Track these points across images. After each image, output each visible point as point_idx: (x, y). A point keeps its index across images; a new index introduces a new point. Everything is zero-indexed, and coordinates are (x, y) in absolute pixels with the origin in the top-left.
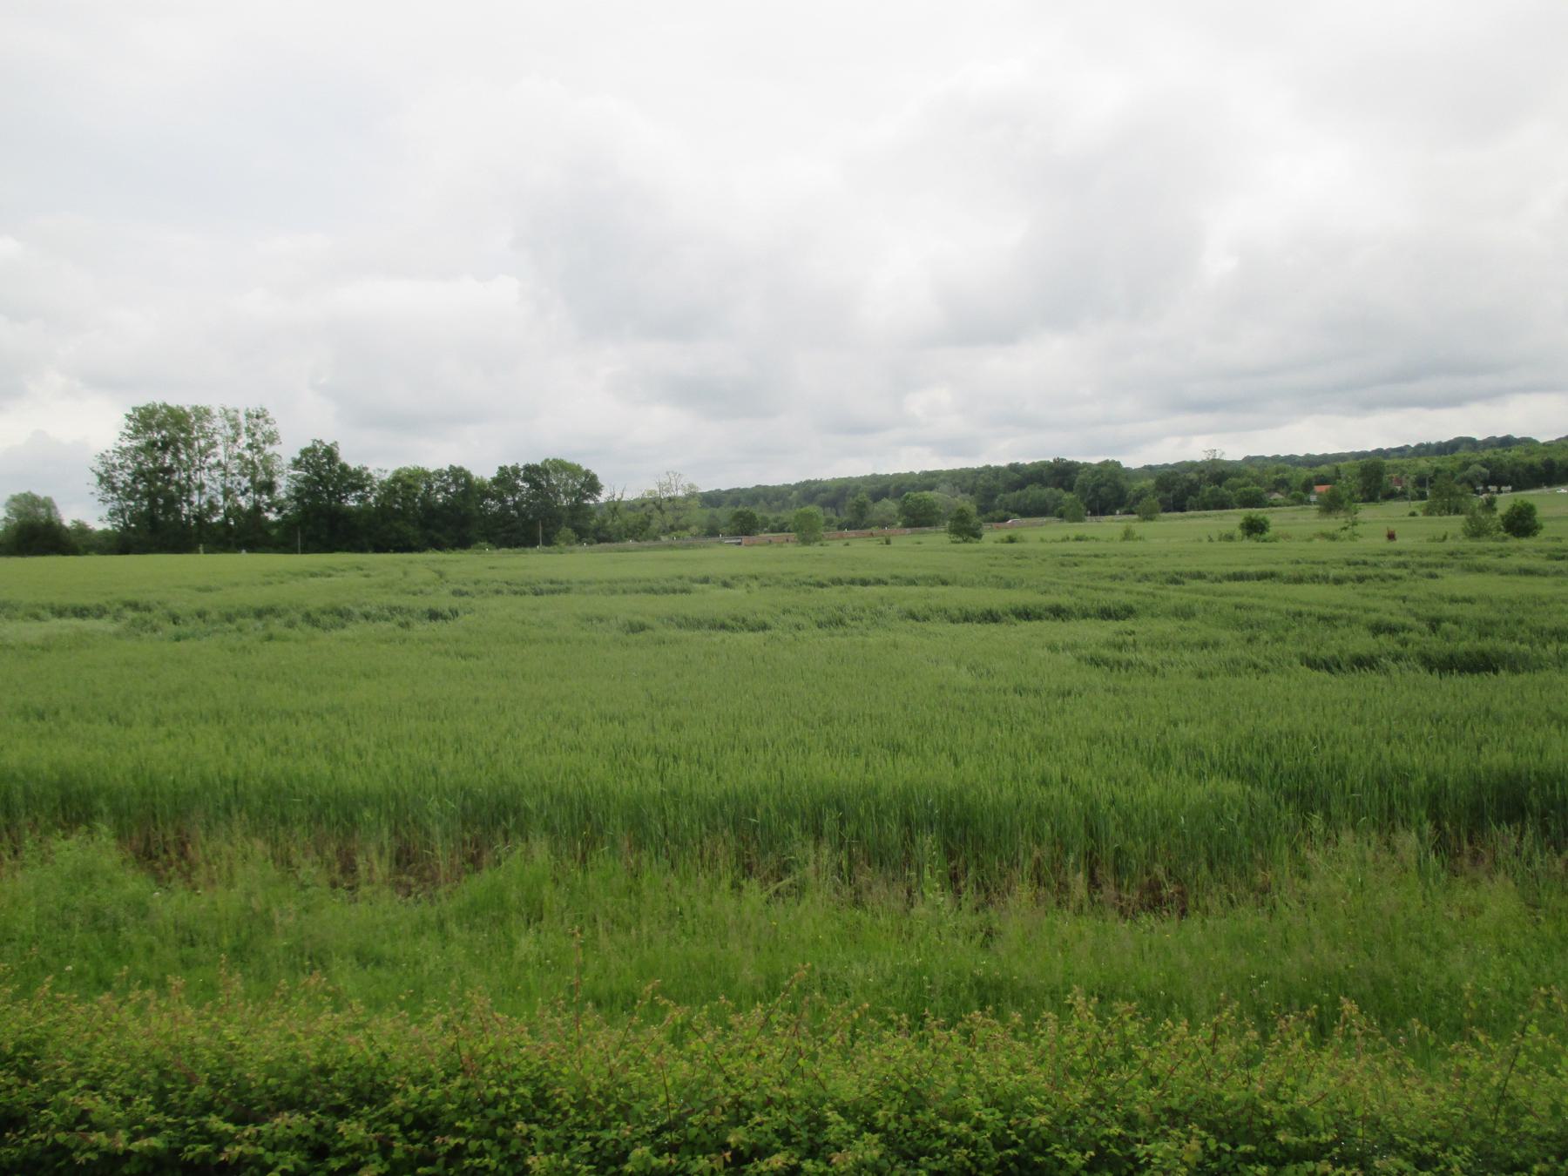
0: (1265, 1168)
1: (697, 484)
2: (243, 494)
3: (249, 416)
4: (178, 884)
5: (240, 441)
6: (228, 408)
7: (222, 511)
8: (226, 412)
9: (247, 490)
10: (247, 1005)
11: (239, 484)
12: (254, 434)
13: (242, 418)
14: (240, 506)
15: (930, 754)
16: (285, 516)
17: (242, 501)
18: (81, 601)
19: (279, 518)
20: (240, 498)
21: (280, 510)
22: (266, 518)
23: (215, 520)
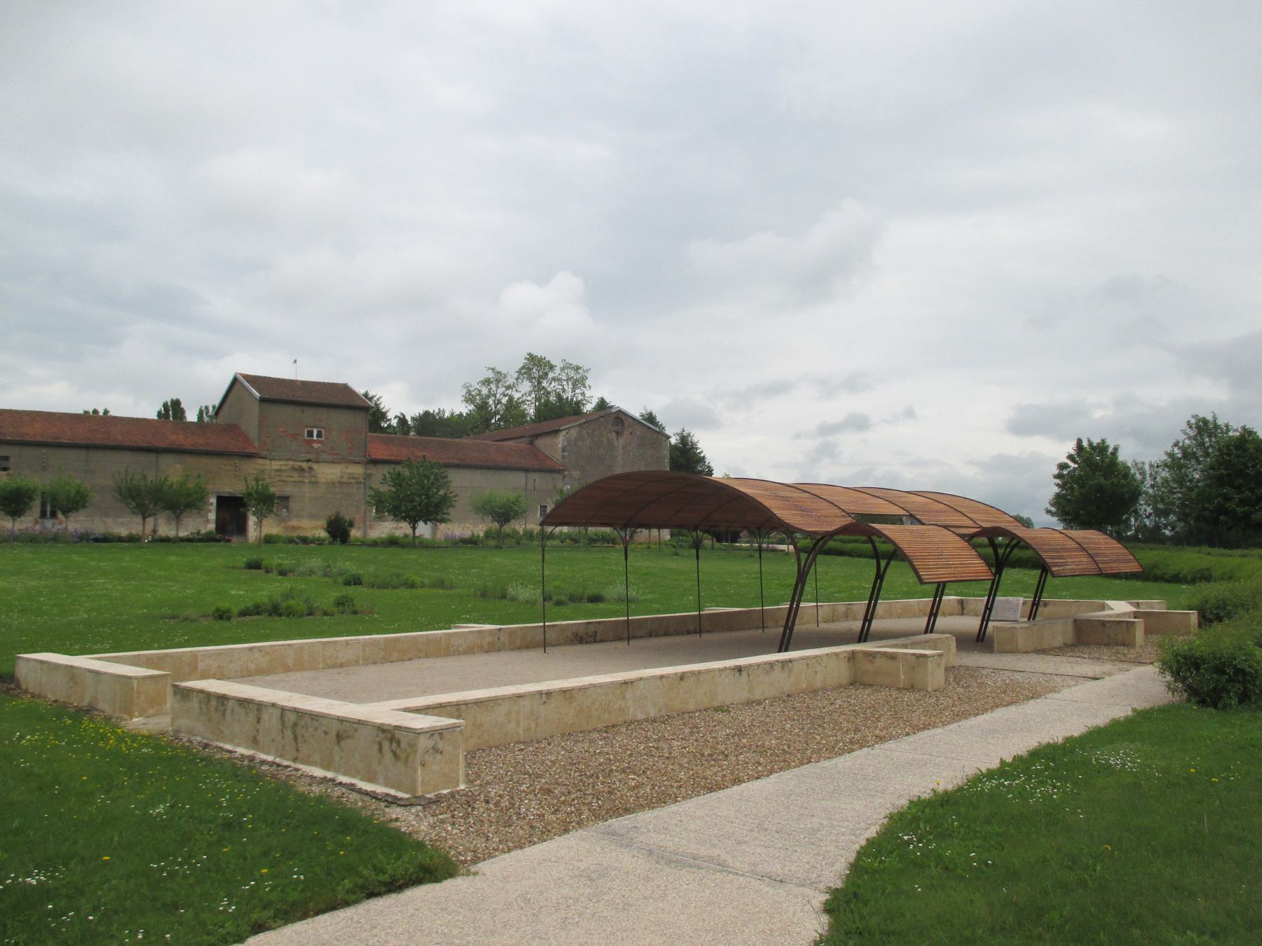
0: (578, 473)
1: (1041, 740)
2: (1148, 517)
3: (1151, 466)
4: (476, 535)
5: (1146, 483)
6: (1138, 461)
7: (1133, 528)
8: (1136, 464)
9: (1150, 514)
10: (1192, 673)
11: (1145, 510)
12: (1155, 478)
13: (1147, 467)
14: (1145, 525)
15: (546, 936)
16: (1177, 532)
17: (1147, 522)
18: (190, 544)
19: (1173, 533)
20: (1146, 520)
21: (1173, 529)
22: (1164, 533)
23: (1129, 534)
